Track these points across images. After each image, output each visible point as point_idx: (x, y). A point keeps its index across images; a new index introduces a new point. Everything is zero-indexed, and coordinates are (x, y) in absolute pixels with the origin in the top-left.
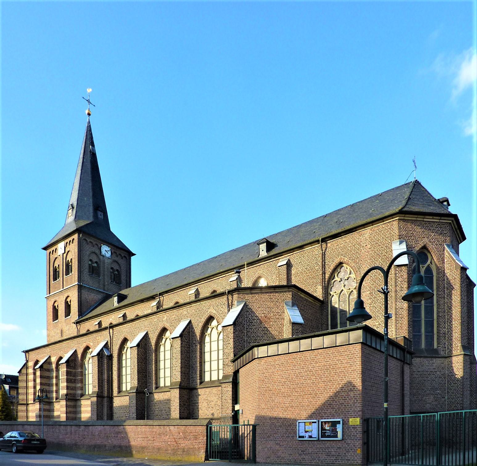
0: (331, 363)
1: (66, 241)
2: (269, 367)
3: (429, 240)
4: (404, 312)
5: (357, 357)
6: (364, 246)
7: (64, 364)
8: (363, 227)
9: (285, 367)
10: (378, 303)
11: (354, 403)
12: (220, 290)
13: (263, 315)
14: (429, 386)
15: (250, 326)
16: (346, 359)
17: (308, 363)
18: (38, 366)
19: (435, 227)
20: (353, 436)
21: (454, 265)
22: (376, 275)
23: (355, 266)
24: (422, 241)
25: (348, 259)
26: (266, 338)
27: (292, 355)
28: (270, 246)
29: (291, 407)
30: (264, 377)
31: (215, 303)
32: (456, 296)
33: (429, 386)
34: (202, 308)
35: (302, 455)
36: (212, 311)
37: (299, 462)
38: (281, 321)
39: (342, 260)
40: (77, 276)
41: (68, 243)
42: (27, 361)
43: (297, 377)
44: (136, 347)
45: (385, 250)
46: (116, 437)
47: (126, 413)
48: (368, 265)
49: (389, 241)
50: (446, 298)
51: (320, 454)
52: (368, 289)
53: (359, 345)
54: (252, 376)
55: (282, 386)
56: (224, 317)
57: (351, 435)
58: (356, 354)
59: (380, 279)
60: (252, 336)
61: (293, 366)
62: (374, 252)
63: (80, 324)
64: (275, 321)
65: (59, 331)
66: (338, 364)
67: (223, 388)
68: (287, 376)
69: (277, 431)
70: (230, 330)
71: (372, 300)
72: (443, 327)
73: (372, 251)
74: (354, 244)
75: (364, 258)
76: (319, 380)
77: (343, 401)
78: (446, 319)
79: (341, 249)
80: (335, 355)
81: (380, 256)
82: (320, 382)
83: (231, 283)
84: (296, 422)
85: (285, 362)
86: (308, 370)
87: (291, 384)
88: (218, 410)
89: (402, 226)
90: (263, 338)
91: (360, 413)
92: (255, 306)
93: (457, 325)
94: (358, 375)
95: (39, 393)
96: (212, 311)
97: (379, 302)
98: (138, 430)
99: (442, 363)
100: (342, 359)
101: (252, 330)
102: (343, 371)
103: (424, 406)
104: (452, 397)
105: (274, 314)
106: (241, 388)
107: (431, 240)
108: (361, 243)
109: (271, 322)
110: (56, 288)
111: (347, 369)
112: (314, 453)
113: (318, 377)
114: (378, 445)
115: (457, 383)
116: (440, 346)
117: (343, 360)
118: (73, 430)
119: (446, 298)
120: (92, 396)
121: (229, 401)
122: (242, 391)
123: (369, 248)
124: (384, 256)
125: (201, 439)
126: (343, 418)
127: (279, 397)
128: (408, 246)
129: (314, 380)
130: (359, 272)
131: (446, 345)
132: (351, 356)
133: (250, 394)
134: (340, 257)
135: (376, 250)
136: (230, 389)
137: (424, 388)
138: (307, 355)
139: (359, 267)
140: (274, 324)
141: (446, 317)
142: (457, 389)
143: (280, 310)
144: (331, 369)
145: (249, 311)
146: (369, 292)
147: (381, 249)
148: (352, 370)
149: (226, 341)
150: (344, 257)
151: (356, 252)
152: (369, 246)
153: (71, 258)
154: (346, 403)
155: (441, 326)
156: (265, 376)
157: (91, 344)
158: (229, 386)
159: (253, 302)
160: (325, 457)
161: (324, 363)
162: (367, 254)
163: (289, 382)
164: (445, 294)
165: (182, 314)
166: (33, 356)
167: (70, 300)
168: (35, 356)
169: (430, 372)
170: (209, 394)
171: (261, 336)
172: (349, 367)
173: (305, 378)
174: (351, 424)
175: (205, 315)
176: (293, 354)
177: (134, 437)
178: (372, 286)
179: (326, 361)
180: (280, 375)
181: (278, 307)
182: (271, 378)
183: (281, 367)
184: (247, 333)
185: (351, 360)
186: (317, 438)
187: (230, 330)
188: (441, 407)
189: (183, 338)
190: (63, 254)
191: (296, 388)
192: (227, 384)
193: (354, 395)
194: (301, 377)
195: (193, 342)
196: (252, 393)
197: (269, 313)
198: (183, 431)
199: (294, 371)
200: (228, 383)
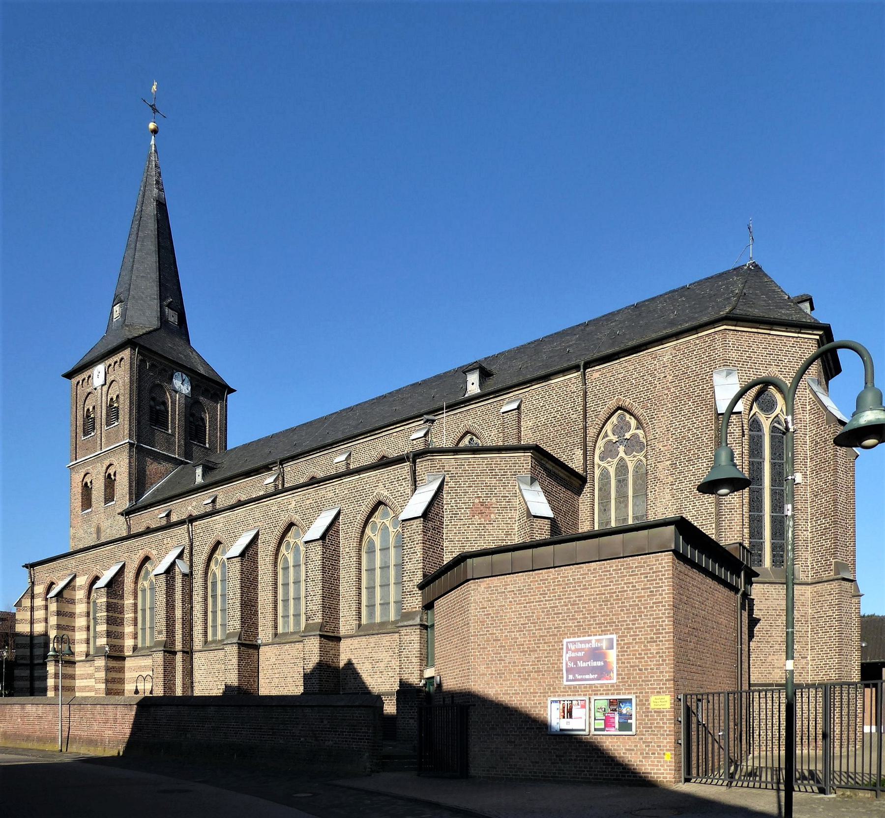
0: (613, 589)
1: (108, 362)
2: (494, 596)
3: (779, 369)
4: (735, 499)
5: (663, 577)
6: (661, 377)
7: (102, 590)
8: (659, 343)
9: (525, 596)
10: (686, 483)
11: (658, 665)
12: (393, 454)
13: (477, 501)
14: (778, 636)
15: (453, 521)
16: (642, 582)
17: (569, 589)
18: (53, 593)
19: (790, 346)
20: (655, 727)
21: (825, 417)
22: (683, 430)
23: (645, 414)
24: (767, 372)
25: (631, 401)
26: (483, 544)
27: (538, 574)
28: (485, 375)
29: (535, 672)
30: (485, 615)
31: (387, 477)
32: (827, 473)
33: (778, 636)
34: (363, 487)
35: (558, 763)
36: (383, 492)
37: (552, 777)
38: (511, 513)
39: (620, 404)
40: (127, 426)
41: (86, 381)
42: (33, 583)
43: (548, 615)
44: (238, 558)
45: (700, 386)
46: (202, 726)
47: (218, 683)
48: (667, 413)
49: (708, 368)
50: (808, 477)
51: (591, 761)
52: (669, 456)
53: (667, 555)
54: (461, 614)
55: (519, 631)
56: (404, 503)
57: (665, 726)
58: (661, 571)
59: (691, 438)
60: (457, 539)
61: (541, 594)
62: (679, 389)
63: (130, 516)
64: (500, 513)
65: (93, 530)
66: (627, 591)
67: (402, 635)
68: (529, 613)
69: (508, 717)
70: (417, 527)
71: (675, 477)
72: (804, 529)
73: (675, 387)
74: (642, 375)
75: (661, 400)
76: (589, 621)
77: (637, 661)
78: (809, 514)
79: (619, 382)
80: (621, 573)
81: (690, 397)
82: (592, 624)
83: (415, 442)
84: (547, 700)
85: (524, 586)
86: (569, 602)
87: (537, 628)
88: (392, 677)
89: (730, 343)
90: (477, 543)
91: (670, 684)
92: (462, 483)
93: (829, 525)
94: (667, 611)
95: (55, 644)
96: (382, 492)
97: (688, 480)
98: (244, 714)
99: (802, 595)
100: (634, 581)
101: (457, 529)
102: (637, 605)
103: (770, 673)
104: (820, 658)
105: (497, 499)
106: (438, 636)
107: (783, 370)
108: (656, 372)
109: (491, 513)
110: (88, 450)
111: (645, 600)
112: (581, 760)
113: (589, 616)
114: (852, 729)
115: (828, 632)
116: (799, 564)
117: (636, 582)
118: (118, 713)
119: (808, 477)
120: (154, 649)
121: (413, 661)
122: (439, 641)
123: (670, 381)
124: (698, 396)
125: (363, 732)
126: (637, 693)
127: (513, 653)
128: (742, 379)
129: (581, 620)
130: (650, 426)
131: (809, 563)
132: (653, 576)
133: (456, 647)
134: (617, 397)
135: (683, 385)
136: (416, 639)
137: (769, 640)
138: (568, 573)
139: (651, 416)
140: (497, 517)
141: (809, 511)
142: (828, 643)
143: (508, 491)
144: (614, 600)
145: (451, 493)
146: (670, 462)
147: (692, 383)
148: (653, 603)
149: (409, 548)
150: (624, 397)
151: (646, 389)
152: (671, 377)
153: (117, 393)
154: (642, 666)
155: (800, 527)
156: (486, 613)
157: (153, 553)
158: (415, 632)
159: (458, 476)
160: (601, 768)
161: (600, 588)
162: (666, 392)
163: (532, 625)
164: (808, 468)
165: (324, 497)
166: (43, 574)
167: (115, 472)
168: (48, 575)
169: (780, 610)
170: (375, 647)
171: (474, 541)
172: (648, 596)
173: (564, 616)
174: (652, 706)
175: (369, 500)
176: (541, 571)
177: (235, 728)
178: (675, 452)
179: (603, 584)
180: (515, 611)
181: (504, 487)
182: (497, 617)
183: (518, 597)
184: (447, 533)
185: (652, 584)
186: (587, 730)
187: (417, 527)
188: (801, 676)
189: (327, 542)
190: (103, 385)
191: (546, 636)
192: (410, 629)
193: (659, 649)
194: (555, 616)
195: (345, 551)
196: (460, 646)
197: (488, 497)
198: (329, 716)
199: (542, 603)
200: (412, 628)
